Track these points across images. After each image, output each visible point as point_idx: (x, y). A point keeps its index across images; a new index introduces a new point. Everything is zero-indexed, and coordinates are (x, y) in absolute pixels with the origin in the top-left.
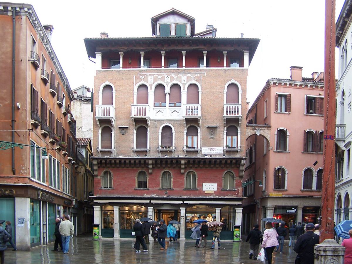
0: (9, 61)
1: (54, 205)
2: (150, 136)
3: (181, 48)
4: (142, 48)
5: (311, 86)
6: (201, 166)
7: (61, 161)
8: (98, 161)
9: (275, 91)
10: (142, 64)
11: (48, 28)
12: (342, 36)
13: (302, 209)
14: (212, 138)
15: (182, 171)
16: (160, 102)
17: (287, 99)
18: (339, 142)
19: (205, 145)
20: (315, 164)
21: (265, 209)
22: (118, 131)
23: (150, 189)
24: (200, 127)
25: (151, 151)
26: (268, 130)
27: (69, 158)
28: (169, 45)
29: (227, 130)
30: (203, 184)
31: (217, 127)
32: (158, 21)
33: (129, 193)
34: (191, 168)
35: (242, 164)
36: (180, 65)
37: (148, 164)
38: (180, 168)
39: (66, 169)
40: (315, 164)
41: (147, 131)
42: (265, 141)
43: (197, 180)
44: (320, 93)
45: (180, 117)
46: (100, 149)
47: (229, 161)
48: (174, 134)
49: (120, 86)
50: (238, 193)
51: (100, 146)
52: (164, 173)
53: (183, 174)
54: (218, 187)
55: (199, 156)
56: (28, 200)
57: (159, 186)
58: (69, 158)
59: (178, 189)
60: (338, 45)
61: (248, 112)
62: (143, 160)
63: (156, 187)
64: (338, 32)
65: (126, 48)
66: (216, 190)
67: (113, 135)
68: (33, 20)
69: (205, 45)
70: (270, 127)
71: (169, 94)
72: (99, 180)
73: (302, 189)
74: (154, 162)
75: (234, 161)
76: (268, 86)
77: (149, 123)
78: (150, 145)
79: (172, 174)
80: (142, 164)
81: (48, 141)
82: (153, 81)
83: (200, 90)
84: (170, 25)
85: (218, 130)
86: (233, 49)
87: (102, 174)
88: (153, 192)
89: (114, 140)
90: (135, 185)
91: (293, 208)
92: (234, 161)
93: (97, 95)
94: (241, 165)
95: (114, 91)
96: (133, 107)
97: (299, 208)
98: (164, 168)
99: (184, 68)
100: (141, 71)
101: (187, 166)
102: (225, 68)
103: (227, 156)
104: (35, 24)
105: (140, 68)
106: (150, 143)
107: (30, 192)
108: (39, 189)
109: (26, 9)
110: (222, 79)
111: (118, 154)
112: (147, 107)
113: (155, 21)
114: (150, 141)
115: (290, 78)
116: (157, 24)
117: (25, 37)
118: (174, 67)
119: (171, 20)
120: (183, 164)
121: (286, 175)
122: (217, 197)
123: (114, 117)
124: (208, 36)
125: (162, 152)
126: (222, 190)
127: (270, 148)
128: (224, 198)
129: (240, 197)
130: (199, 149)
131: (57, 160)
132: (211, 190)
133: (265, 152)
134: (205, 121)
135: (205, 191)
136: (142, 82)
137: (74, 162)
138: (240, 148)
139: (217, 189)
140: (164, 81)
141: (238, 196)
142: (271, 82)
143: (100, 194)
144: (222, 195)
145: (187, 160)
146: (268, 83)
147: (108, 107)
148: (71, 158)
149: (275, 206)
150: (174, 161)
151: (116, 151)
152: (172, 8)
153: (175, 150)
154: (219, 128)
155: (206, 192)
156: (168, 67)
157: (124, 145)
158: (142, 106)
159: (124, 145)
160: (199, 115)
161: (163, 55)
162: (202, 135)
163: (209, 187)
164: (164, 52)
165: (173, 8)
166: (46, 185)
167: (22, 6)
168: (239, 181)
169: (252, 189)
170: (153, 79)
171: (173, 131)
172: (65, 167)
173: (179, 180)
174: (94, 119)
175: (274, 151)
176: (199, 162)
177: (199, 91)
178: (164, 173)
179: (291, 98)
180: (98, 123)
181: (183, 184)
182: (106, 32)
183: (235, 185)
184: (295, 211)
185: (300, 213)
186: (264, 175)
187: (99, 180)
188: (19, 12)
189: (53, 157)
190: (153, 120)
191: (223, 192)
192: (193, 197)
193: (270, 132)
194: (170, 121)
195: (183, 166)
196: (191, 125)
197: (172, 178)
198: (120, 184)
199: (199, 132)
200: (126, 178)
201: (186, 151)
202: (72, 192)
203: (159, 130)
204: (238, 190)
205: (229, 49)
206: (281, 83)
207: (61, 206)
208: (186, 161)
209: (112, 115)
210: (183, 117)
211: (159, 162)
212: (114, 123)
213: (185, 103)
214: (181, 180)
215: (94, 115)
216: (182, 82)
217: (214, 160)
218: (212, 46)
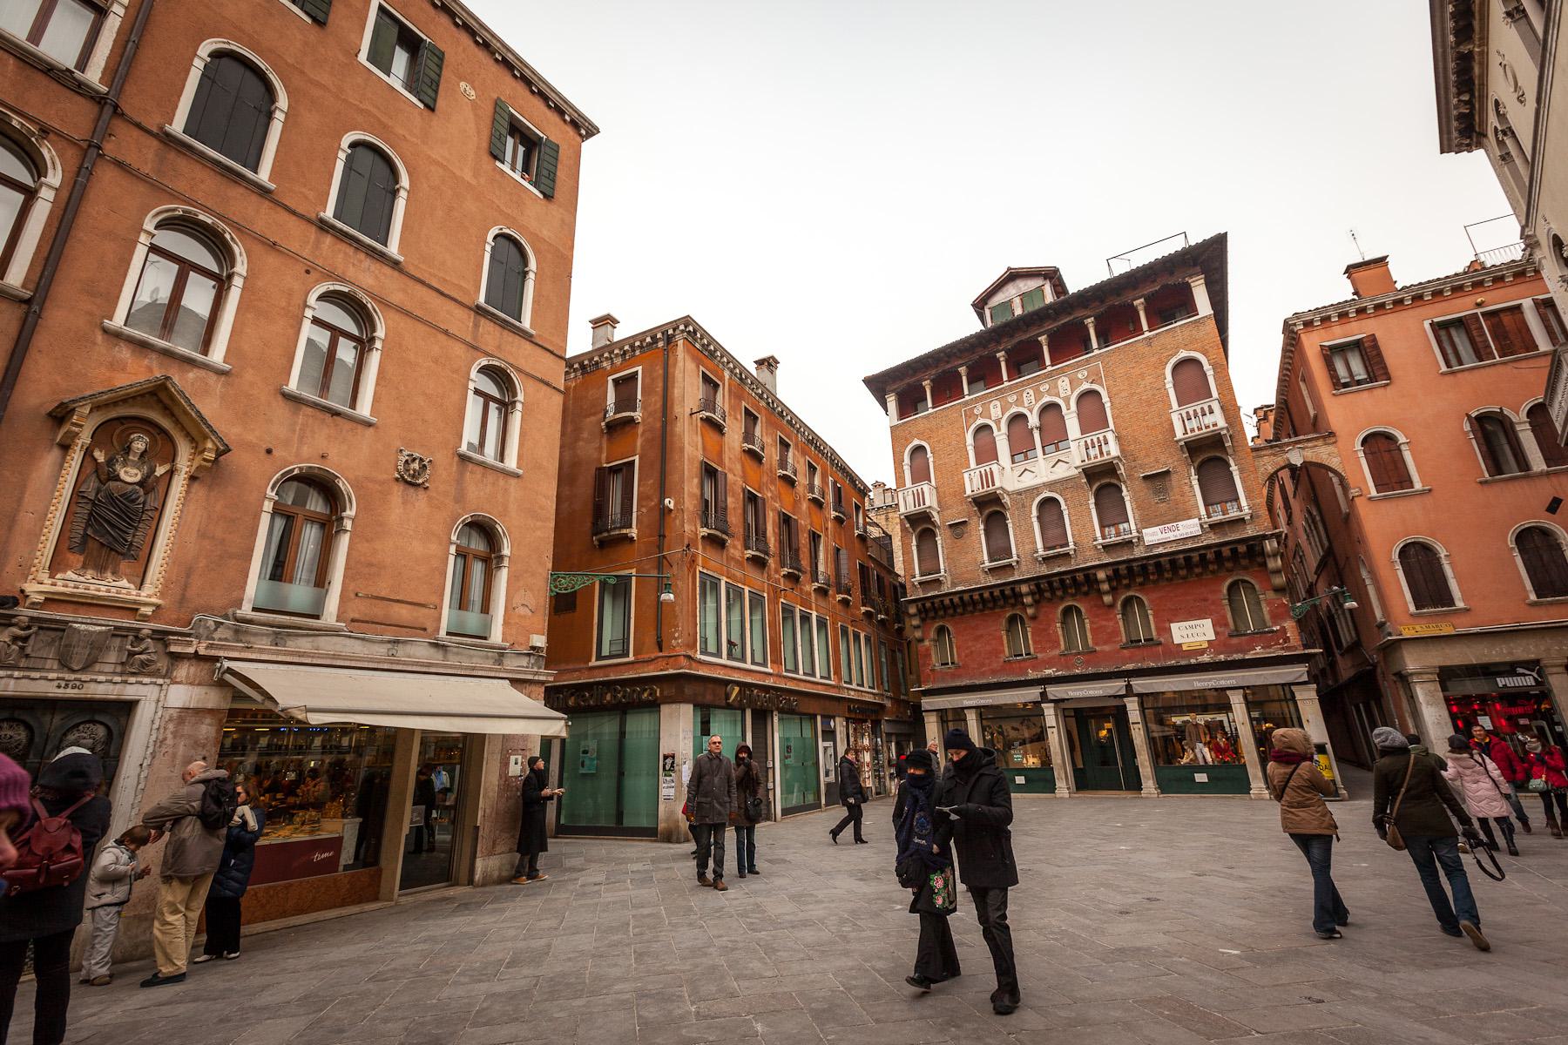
0: (658, 425)
4: (960, 362)
9: (1312, 343)
11: (768, 363)
12: (1477, 106)
14: (1163, 501)
15: (1107, 599)
16: (1021, 449)
17: (1369, 350)
19: (1147, 521)
22: (948, 532)
24: (1125, 482)
26: (1329, 444)
28: (1012, 336)
29: (1198, 472)
30: (1172, 625)
31: (1167, 472)
33: (994, 672)
34: (1128, 587)
35: (1270, 553)
36: (1087, 348)
38: (1100, 593)
41: (1006, 519)
42: (1335, 480)
43: (1151, 617)
44: (1479, 300)
46: (918, 578)
47: (1226, 551)
48: (1066, 513)
50: (1287, 640)
52: (1067, 612)
53: (1112, 606)
54: (1218, 629)
55: (1138, 552)
56: (691, 706)
57: (1059, 645)
59: (1107, 648)
60: (1475, 140)
61: (1275, 428)
62: (1009, 588)
63: (1052, 648)
64: (1455, 101)
65: (934, 372)
67: (939, 542)
68: (703, 345)
69: (1086, 307)
70: (1332, 434)
71: (1040, 429)
72: (928, 649)
75: (1242, 549)
76: (1294, 339)
77: (1006, 500)
78: (1017, 549)
79: (1083, 610)
80: (1010, 598)
81: (777, 572)
82: (1000, 413)
83: (1105, 399)
84: (1011, 301)
85: (1174, 477)
86: (1157, 288)
87: (932, 634)
88: (1049, 663)
91: (1520, 670)
92: (1242, 549)
94: (1269, 556)
95: (929, 455)
97: (1546, 667)
98: (1062, 599)
100: (966, 403)
104: (710, 351)
106: (1017, 545)
107: (688, 690)
108: (727, 682)
109: (682, 327)
111: (954, 584)
112: (995, 468)
114: (1016, 541)
117: (681, 375)
119: (1011, 292)
120: (1103, 582)
122: (1222, 657)
123: (935, 505)
125: (1046, 559)
126: (1231, 636)
127: (1353, 492)
128: (1244, 660)
129: (1296, 649)
130: (1247, 511)
133: (1344, 508)
134: (1133, 464)
135: (1180, 645)
136: (980, 421)
138: (1250, 509)
139: (1216, 633)
140: (1022, 404)
141: (1288, 649)
142: (1295, 324)
143: (933, 682)
145: (1110, 568)
146: (1288, 328)
147: (988, 469)
150: (1080, 577)
151: (949, 578)
153: (1075, 550)
154: (1176, 472)
155: (1185, 648)
157: (963, 561)
159: (963, 561)
162: (1135, 499)
163: (1190, 632)
165: (1009, 269)
166: (771, 671)
167: (674, 325)
168: (1278, 602)
169: (1350, 624)
171: (1063, 507)
172: (850, 629)
173: (1104, 623)
175: (1370, 499)
176: (1144, 568)
177: (1104, 401)
178: (1067, 612)
179: (1380, 344)
180: (908, 525)
181: (1116, 632)
183: (1267, 617)
184: (1535, 679)
186: (1364, 574)
187: (928, 649)
188: (674, 336)
190: (1014, 493)
191: (1235, 641)
192: (1152, 664)
194: (1050, 485)
195: (1105, 587)
196: (1103, 482)
197: (1087, 621)
198: (972, 652)
200: (982, 636)
204: (1284, 630)
206: (1329, 318)
207: (837, 719)
208: (1110, 572)
209: (931, 500)
211: (1044, 586)
212: (936, 518)
213: (1078, 435)
214: (1111, 624)
216: (1062, 395)
218: (1102, 302)
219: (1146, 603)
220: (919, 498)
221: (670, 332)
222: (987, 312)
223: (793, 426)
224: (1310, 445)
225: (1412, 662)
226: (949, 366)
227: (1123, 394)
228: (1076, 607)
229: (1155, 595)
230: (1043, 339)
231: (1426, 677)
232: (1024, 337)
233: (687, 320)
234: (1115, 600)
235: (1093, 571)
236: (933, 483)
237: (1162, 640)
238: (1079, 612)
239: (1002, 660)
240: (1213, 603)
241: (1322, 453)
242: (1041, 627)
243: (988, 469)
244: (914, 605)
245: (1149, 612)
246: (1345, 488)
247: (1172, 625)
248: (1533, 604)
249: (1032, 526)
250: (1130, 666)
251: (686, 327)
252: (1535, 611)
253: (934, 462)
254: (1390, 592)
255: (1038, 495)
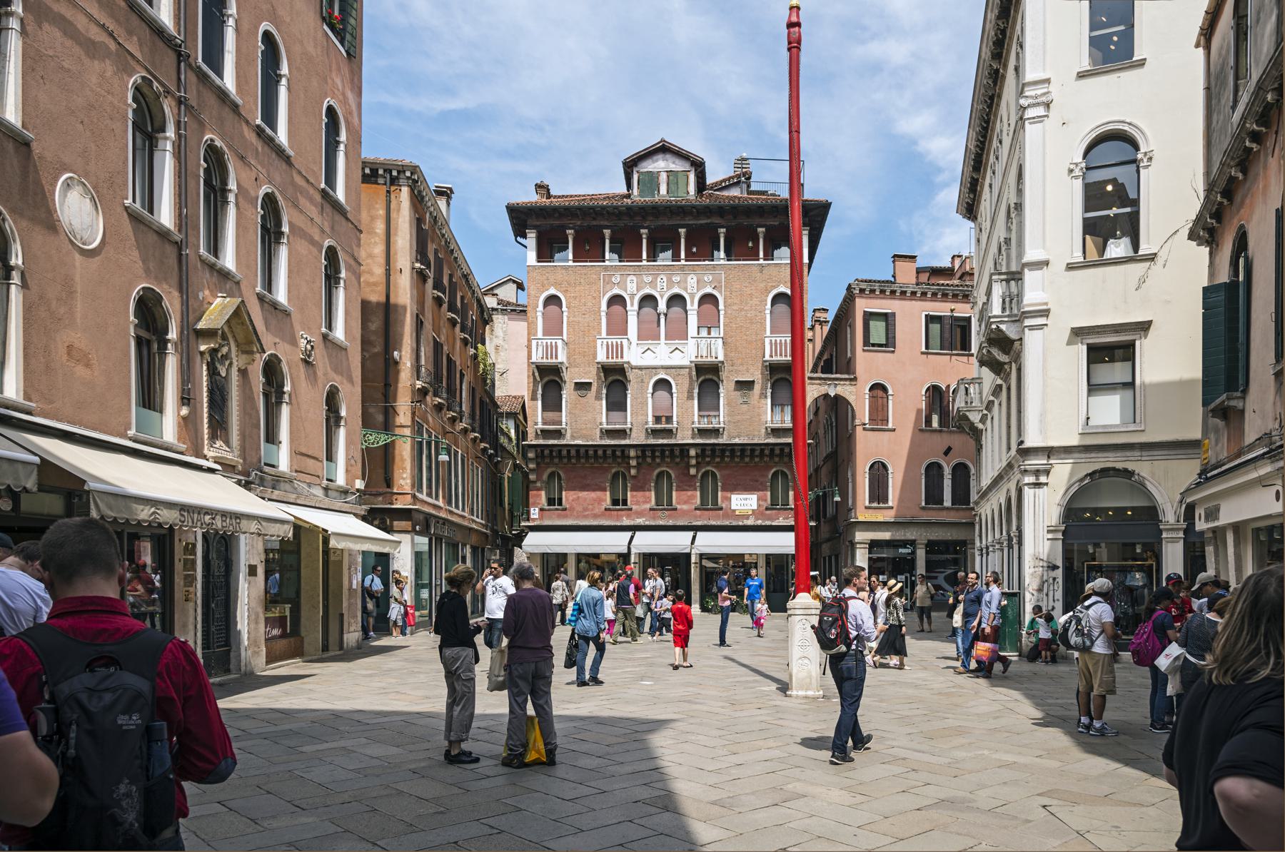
1: (455, 546)
2: (632, 401)
3: (678, 222)
4: (606, 223)
5: (934, 294)
6: (666, 459)
7: (467, 454)
8: (536, 451)
10: (607, 255)
11: (446, 193)
13: (923, 546)
14: (745, 403)
16: (648, 334)
18: (972, 412)
20: (946, 453)
21: (853, 545)
23: (634, 507)
25: (634, 430)
27: (483, 445)
29: (772, 388)
32: (636, 166)
33: (595, 516)
34: (708, 464)
36: (676, 257)
37: (629, 457)
38: (688, 466)
39: (477, 468)
40: (946, 453)
45: (686, 362)
49: (575, 298)
51: (540, 420)
57: (650, 500)
58: (483, 445)
59: (685, 507)
65: (579, 223)
66: (755, 507)
71: (666, 315)
73: (923, 504)
74: (699, 451)
82: (635, 289)
83: (721, 306)
86: (776, 223)
88: (640, 514)
89: (566, 406)
90: (605, 500)
93: (533, 315)
95: (564, 308)
96: (599, 342)
99: (683, 262)
100: (606, 268)
101: (700, 460)
102: (761, 261)
103: (772, 440)
105: (604, 261)
109: (408, 174)
110: (762, 285)
111: (573, 437)
112: (625, 342)
113: (630, 165)
115: (893, 280)
116: (635, 172)
118: (665, 258)
119: (660, 165)
120: (692, 457)
121: (890, 476)
122: (759, 522)
124: (735, 192)
128: (771, 526)
130: (722, 425)
131: (460, 452)
132: (746, 508)
135: (734, 511)
136: (616, 291)
137: (492, 451)
140: (655, 288)
144: (768, 519)
145: (700, 447)
146: (849, 288)
147: (554, 341)
148: (487, 446)
149: (871, 540)
152: (659, 140)
155: (737, 513)
156: (655, 261)
158: (615, 340)
160: (721, 358)
161: (644, 236)
162: (727, 397)
163: (743, 502)
164: (646, 231)
170: (635, 285)
172: (475, 464)
174: (530, 364)
176: (723, 451)
182: (546, 182)
185: (921, 554)
186: (849, 474)
189: (454, 447)
193: (854, 390)
194: (666, 368)
195: (693, 462)
196: (707, 377)
197: (674, 484)
199: (721, 390)
201: (652, 431)
202: (488, 515)
203: (648, 387)
205: (768, 223)
210: (691, 362)
215: (529, 357)
217: (749, 448)
218: (735, 217)
219: (718, 477)
220: (551, 350)
221: (395, 173)
222: (635, 177)
223: (456, 262)
224: (842, 383)
225: (860, 536)
226: (594, 223)
227: (735, 307)
228: (667, 472)
229: (726, 472)
230: (682, 231)
231: (862, 546)
232: (667, 223)
233: (414, 169)
234: (697, 472)
235: (687, 447)
236: (565, 337)
237: (724, 506)
238: (669, 476)
239: (603, 507)
240: (761, 484)
241: (844, 390)
242: (639, 484)
243: (619, 341)
244: (533, 450)
245: (719, 484)
246: (854, 417)
247: (733, 496)
248: (923, 508)
249: (647, 401)
250: (699, 523)
251: (412, 174)
252: (922, 513)
253: (568, 317)
254: (859, 491)
255: (656, 374)
